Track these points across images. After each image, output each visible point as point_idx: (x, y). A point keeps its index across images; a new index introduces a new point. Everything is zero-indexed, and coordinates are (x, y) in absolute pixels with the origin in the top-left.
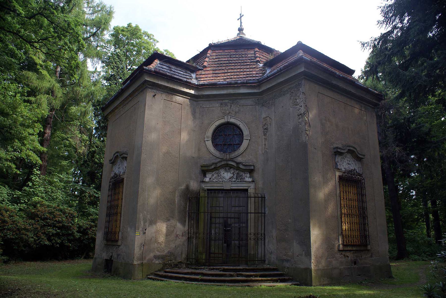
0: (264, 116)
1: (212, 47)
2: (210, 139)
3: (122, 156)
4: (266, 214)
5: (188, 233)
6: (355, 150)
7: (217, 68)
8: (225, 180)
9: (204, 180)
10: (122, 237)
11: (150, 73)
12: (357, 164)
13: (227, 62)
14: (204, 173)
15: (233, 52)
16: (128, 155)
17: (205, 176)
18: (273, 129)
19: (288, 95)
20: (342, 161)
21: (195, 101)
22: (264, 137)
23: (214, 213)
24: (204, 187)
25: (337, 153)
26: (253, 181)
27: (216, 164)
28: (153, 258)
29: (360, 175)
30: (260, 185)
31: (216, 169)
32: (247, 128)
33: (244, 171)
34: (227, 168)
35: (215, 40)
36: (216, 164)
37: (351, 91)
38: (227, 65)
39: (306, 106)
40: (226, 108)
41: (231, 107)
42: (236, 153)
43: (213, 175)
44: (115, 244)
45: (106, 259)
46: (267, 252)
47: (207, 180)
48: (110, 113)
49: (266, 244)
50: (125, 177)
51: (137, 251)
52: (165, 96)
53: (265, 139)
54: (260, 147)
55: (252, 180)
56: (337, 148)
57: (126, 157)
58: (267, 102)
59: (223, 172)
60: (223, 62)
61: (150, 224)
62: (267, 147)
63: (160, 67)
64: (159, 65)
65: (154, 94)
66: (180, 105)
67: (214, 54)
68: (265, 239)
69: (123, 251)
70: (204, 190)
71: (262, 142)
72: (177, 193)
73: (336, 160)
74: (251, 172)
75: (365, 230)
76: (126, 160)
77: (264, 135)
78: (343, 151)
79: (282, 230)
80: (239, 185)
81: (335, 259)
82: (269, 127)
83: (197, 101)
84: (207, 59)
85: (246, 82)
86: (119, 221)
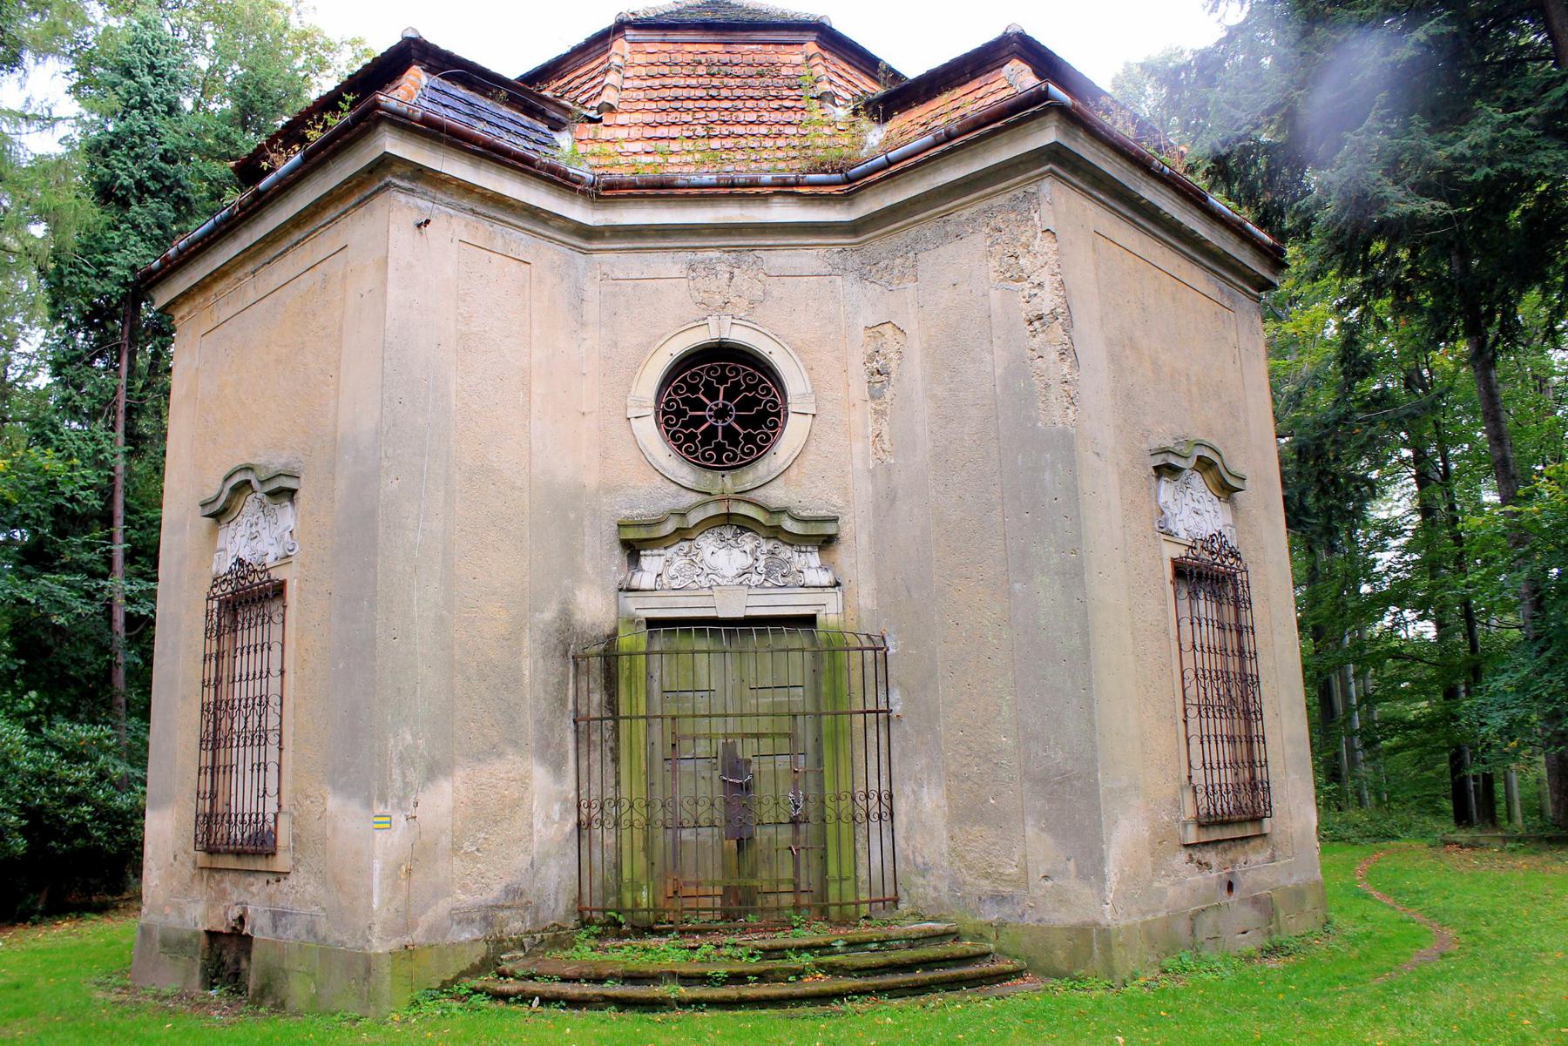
2: (651, 411)
3: (274, 485)
4: (893, 715)
5: (579, 806)
6: (1216, 459)
7: (658, 118)
8: (720, 581)
9: (635, 584)
10: (296, 838)
11: (403, 123)
12: (1220, 514)
13: (702, 93)
14: (633, 550)
15: (715, 51)
16: (302, 479)
18: (913, 372)
23: (703, 716)
24: (633, 609)
27: (683, 515)
28: (449, 922)
31: (682, 534)
32: (803, 369)
33: (795, 540)
34: (728, 533)
37: (1195, 232)
39: (1062, 283)
41: (731, 278)
43: (669, 562)
44: (260, 864)
45: (208, 932)
46: (903, 866)
47: (645, 579)
48: (187, 295)
50: (288, 574)
51: (379, 899)
52: (462, 227)
53: (879, 413)
54: (858, 447)
55: (832, 580)
57: (293, 492)
58: (882, 265)
59: (712, 549)
61: (428, 779)
62: (885, 447)
66: (523, 265)
68: (892, 815)
69: (308, 897)
70: (632, 621)
71: (865, 425)
72: (526, 642)
73: (1162, 500)
74: (826, 543)
76: (292, 500)
77: (873, 397)
79: (968, 778)
81: (1172, 878)
82: (893, 365)
83: (590, 252)
86: (272, 769)
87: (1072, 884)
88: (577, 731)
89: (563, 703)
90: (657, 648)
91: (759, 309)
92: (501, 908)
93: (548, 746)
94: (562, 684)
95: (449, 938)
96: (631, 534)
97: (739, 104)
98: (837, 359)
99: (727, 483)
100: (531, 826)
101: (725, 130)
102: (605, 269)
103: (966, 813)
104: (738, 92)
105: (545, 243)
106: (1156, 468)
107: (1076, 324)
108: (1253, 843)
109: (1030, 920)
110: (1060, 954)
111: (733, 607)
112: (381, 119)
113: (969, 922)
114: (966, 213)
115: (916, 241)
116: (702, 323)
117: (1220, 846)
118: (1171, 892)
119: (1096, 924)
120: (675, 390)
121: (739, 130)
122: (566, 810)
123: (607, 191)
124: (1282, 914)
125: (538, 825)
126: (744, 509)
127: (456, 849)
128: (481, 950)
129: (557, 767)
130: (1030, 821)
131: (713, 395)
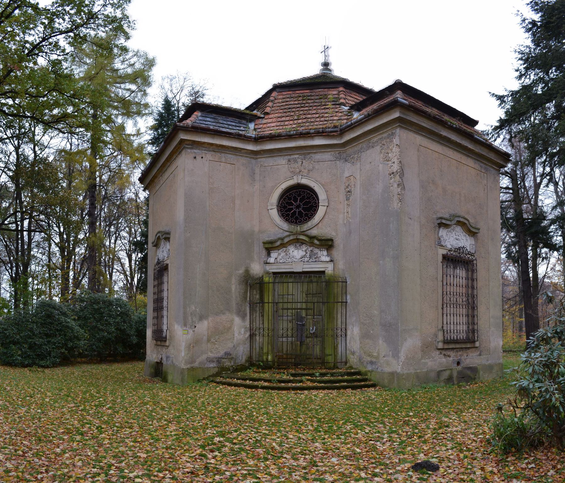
0: (346, 174)
1: (278, 88)
2: (275, 207)
4: (348, 304)
6: (466, 222)
7: (283, 115)
9: (268, 261)
10: (170, 336)
12: (469, 240)
14: (269, 251)
17: (269, 255)
19: (378, 148)
20: (449, 236)
21: (253, 158)
22: (346, 202)
25: (442, 224)
26: (331, 261)
29: (472, 255)
30: (341, 265)
31: (283, 245)
35: (283, 79)
36: (282, 239)
38: (298, 109)
40: (296, 165)
42: (310, 224)
43: (279, 254)
44: (163, 344)
47: (272, 260)
49: (348, 342)
54: (341, 216)
56: (441, 218)
60: (293, 106)
63: (201, 120)
64: (200, 118)
65: (194, 155)
67: (281, 97)
68: (346, 335)
70: (268, 273)
71: (344, 209)
73: (440, 234)
75: (474, 324)
77: (347, 200)
78: (448, 223)
80: (313, 266)
83: (257, 158)
84: (270, 104)
85: (323, 131)
87: (390, 359)
88: (250, 307)
89: (246, 298)
90: (277, 281)
91: (311, 173)
92: (224, 358)
93: (240, 311)
94: (246, 292)
95: (206, 366)
96: (267, 246)
97: (311, 108)
98: (336, 188)
99: (298, 228)
100: (234, 335)
101: (304, 117)
102: (262, 163)
103: (365, 336)
104: (311, 104)
105: (240, 157)
106: (439, 224)
107: (405, 176)
108: (471, 350)
109: (379, 370)
110: (386, 381)
111: (298, 268)
112: (179, 130)
113: (363, 370)
114: (375, 139)
115: (361, 149)
116: (292, 178)
117: (455, 350)
118: (430, 363)
119: (396, 372)
120: (284, 199)
121: (309, 116)
122: (246, 331)
123: (258, 140)
124: (481, 373)
125: (236, 335)
126: (302, 237)
127: (209, 340)
128: (216, 370)
129: (243, 317)
130: (381, 338)
131: (296, 201)
